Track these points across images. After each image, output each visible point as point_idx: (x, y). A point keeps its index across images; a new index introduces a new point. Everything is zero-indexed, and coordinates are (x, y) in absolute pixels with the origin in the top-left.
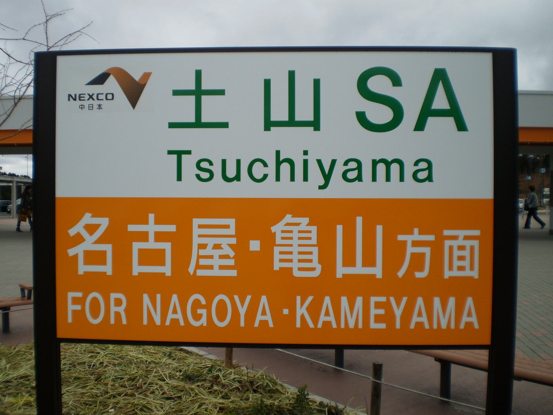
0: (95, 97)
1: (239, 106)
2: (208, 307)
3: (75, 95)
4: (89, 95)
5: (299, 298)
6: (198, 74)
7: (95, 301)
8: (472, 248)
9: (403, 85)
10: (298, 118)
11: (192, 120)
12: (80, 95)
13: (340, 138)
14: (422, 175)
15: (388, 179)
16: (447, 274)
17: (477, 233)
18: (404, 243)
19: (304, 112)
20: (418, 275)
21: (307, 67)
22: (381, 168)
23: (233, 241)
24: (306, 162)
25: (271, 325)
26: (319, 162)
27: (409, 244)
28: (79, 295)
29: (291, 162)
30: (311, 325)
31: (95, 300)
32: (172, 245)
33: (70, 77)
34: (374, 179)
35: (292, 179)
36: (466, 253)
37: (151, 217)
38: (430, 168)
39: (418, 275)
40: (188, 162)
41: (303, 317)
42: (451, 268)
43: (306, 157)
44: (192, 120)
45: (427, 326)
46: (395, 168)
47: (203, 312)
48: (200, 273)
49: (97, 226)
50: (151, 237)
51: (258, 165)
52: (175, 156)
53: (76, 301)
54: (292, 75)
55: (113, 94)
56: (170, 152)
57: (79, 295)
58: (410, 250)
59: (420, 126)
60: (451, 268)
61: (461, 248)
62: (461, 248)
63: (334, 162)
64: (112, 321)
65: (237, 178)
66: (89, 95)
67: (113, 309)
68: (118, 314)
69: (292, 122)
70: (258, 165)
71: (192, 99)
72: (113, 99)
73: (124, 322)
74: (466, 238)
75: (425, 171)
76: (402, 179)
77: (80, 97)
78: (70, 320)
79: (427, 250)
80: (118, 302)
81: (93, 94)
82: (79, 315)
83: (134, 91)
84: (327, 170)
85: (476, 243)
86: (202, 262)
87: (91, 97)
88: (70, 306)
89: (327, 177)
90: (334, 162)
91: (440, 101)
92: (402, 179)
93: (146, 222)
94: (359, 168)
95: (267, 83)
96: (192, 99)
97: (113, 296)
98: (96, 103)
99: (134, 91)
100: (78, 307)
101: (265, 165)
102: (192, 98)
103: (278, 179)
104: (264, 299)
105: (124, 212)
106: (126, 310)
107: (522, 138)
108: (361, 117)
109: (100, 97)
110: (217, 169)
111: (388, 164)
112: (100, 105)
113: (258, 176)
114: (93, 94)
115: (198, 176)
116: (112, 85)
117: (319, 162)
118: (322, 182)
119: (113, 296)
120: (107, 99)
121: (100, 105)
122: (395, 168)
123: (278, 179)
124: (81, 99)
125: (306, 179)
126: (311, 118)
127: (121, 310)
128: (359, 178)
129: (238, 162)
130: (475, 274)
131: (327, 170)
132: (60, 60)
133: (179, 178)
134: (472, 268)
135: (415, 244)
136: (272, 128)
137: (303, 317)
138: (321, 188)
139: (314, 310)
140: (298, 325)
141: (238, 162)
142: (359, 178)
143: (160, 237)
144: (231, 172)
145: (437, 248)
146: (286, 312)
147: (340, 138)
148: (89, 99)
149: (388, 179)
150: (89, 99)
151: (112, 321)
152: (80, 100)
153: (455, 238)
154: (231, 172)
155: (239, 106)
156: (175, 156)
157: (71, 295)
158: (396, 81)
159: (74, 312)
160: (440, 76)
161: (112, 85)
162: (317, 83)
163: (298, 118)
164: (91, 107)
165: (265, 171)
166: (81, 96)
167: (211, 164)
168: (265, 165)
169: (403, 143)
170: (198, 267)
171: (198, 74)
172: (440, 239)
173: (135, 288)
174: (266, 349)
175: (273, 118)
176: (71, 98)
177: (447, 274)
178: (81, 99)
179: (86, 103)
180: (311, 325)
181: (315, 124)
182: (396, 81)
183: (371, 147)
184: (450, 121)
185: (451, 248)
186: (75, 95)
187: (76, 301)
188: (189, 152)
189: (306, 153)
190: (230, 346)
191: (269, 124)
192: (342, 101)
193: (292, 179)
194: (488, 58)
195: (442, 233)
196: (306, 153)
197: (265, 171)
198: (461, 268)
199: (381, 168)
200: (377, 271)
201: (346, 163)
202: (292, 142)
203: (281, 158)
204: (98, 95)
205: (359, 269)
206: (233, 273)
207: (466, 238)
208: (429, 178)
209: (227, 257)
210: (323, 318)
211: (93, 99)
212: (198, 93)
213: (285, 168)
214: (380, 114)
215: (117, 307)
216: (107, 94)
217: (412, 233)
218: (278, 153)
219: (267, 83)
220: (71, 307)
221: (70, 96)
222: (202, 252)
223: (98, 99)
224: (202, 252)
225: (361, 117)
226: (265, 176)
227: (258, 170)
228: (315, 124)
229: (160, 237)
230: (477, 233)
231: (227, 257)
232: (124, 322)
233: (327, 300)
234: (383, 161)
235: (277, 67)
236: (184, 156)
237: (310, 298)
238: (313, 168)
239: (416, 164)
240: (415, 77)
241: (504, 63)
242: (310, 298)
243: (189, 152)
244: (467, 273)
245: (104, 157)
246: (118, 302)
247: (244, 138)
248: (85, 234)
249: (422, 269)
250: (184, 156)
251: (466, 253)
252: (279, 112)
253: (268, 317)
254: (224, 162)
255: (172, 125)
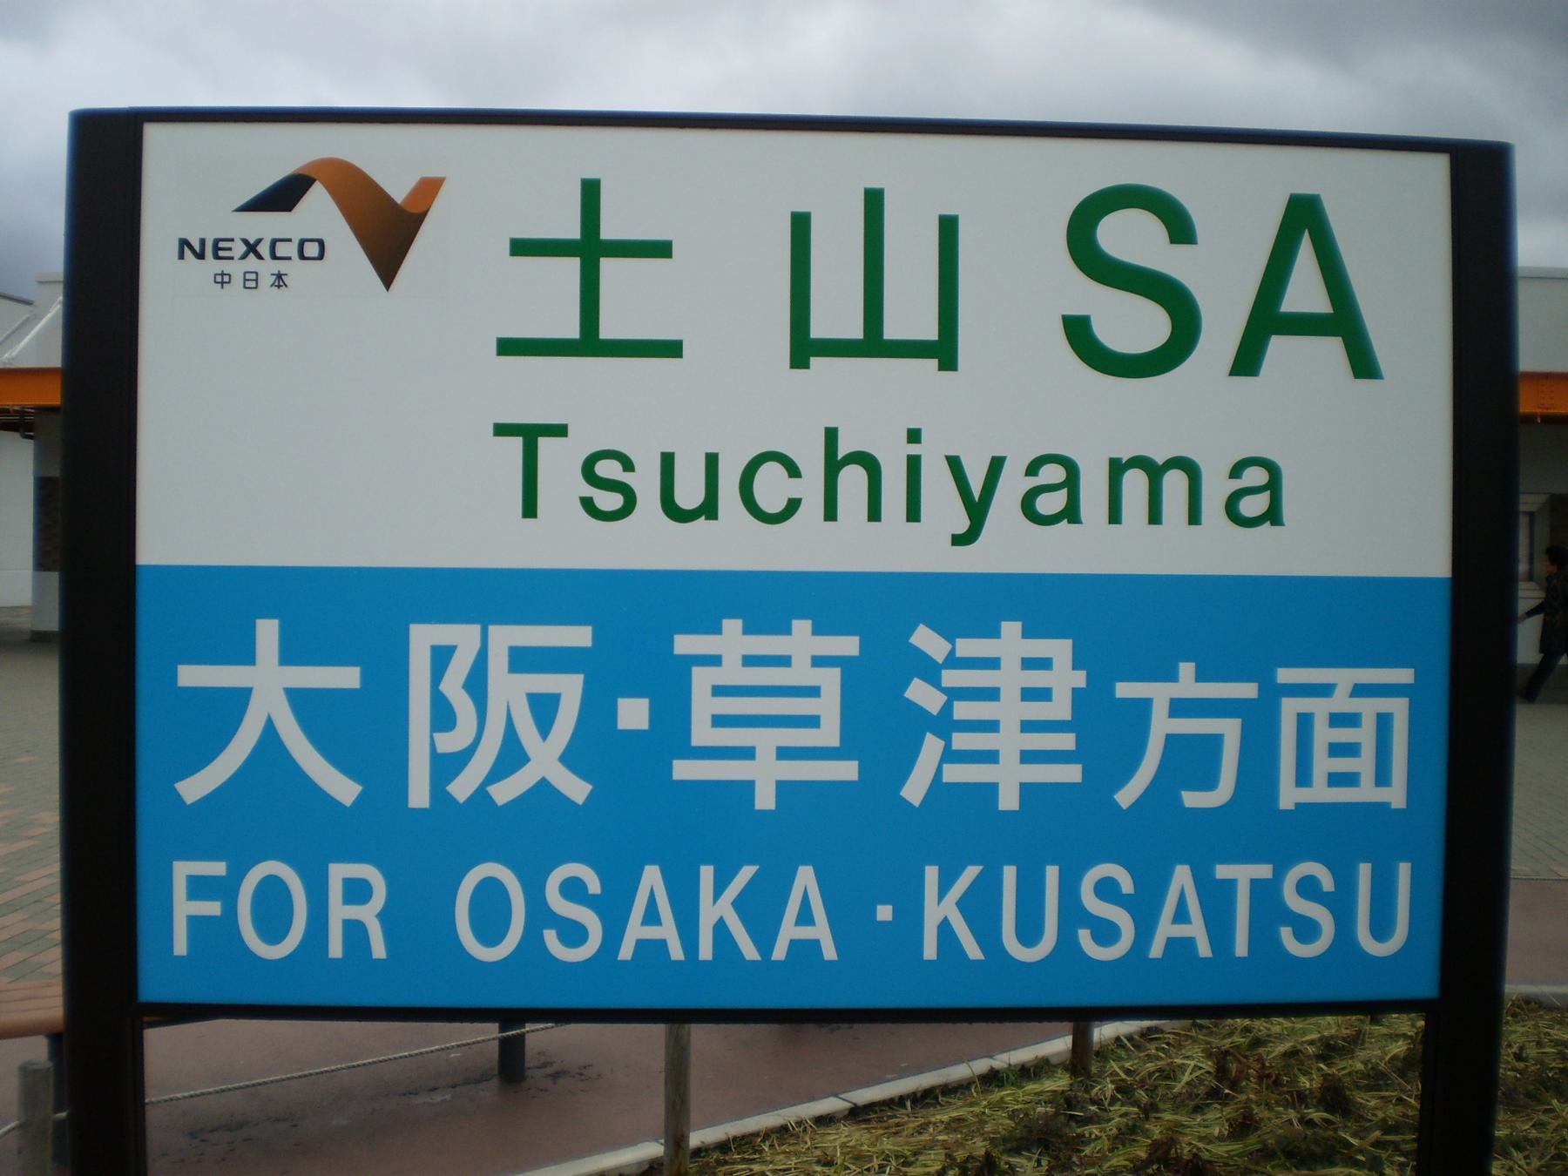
0: (264, 249)
1: (713, 288)
3: (203, 242)
4: (245, 242)
5: (931, 874)
6: (591, 192)
7: (272, 891)
8: (1384, 721)
9: (1199, 239)
10: (891, 332)
11: (572, 331)
12: (217, 241)
13: (1017, 393)
14: (1253, 506)
15: (1155, 517)
16: (1289, 796)
17: (1404, 676)
18: (1143, 707)
19: (909, 316)
20: (1192, 799)
21: (920, 179)
22: (1135, 484)
24: (914, 464)
25: (829, 952)
26: (954, 464)
27: (1159, 712)
28: (218, 868)
29: (870, 464)
30: (750, 952)
31: (491, 887)
32: (651, 704)
33: (181, 191)
34: (1115, 516)
35: (874, 514)
36: (1361, 735)
37: (268, 632)
38: (1274, 485)
39: (1192, 799)
40: (559, 463)
41: (945, 928)
42: (1303, 777)
43: (914, 449)
44: (572, 331)
45: (676, 952)
46: (1175, 483)
51: (771, 470)
52: (517, 442)
53: (200, 888)
54: (874, 202)
55: (321, 243)
56: (502, 430)
57: (218, 868)
58: (1161, 726)
59: (1247, 362)
60: (1303, 777)
63: (996, 465)
64: (336, 949)
65: (709, 509)
66: (245, 242)
67: (339, 912)
68: (354, 931)
69: (873, 344)
70: (771, 470)
71: (571, 266)
72: (321, 257)
73: (379, 950)
74: (1359, 691)
75: (1262, 495)
76: (1194, 517)
77: (216, 249)
78: (181, 946)
79: (1229, 730)
80: (357, 892)
81: (259, 241)
82: (215, 935)
83: (388, 232)
84: (976, 489)
85: (1398, 708)
87: (252, 248)
88: (182, 902)
89: (977, 510)
90: (996, 465)
91: (1305, 292)
92: (1194, 517)
93: (246, 656)
94: (1072, 483)
95: (801, 225)
96: (571, 266)
97: (339, 872)
98: (267, 268)
99: (388, 232)
100: (213, 908)
101: (793, 471)
102: (573, 265)
103: (831, 514)
104: (805, 877)
105: (356, 613)
106: (382, 916)
107: (1528, 403)
108: (1078, 332)
109: (281, 250)
110: (646, 483)
111: (1154, 472)
112: (279, 276)
113: (772, 505)
114: (259, 241)
115: (588, 504)
116: (319, 212)
117: (954, 464)
118: (962, 524)
119: (339, 872)
120: (302, 257)
121: (279, 276)
122: (1175, 483)
123: (831, 514)
124: (221, 253)
125: (913, 514)
126: (930, 332)
127: (368, 914)
128: (1071, 513)
129: (712, 461)
130: (1395, 795)
131: (976, 489)
132: (153, 134)
133: (530, 510)
134: (1382, 778)
135: (1179, 708)
136: (812, 360)
137: (945, 928)
138: (958, 540)
139: (761, 909)
140: (930, 951)
141: (712, 461)
142: (1071, 513)
144: (689, 494)
146: (884, 913)
147: (1017, 393)
148: (244, 257)
149: (1155, 517)
150: (244, 257)
151: (336, 949)
152: (217, 257)
153: (1325, 690)
154: (689, 494)
155: (713, 288)
156: (517, 442)
157: (183, 870)
158: (1180, 229)
159: (194, 922)
160: (1303, 217)
161: (319, 212)
162: (948, 228)
163: (891, 332)
164: (251, 282)
165: (793, 488)
166: (221, 245)
167: (628, 465)
168: (793, 471)
169: (1197, 413)
171: (591, 192)
172: (1272, 694)
173: (425, 849)
174: (963, 1027)
175: (818, 331)
176: (197, 248)
177: (1289, 796)
178: (221, 253)
179: (236, 268)
180: (750, 952)
181: (944, 351)
182: (1180, 229)
183: (1111, 421)
184: (1331, 349)
185: (1305, 722)
186: (203, 242)
187: (200, 888)
188: (560, 431)
189: (914, 436)
190: (676, 1017)
191: (804, 349)
192: (1022, 287)
193: (874, 514)
194: (1439, 166)
195: (1273, 676)
196: (914, 436)
197: (793, 488)
198: (1336, 780)
199: (1135, 484)
201: (1032, 469)
202: (873, 403)
203: (842, 452)
204: (274, 243)
207: (1359, 691)
208: (1273, 515)
210: (789, 931)
211: (260, 257)
212: (591, 249)
213: (853, 480)
214: (1135, 325)
215: (355, 907)
216: (302, 243)
217: (1172, 676)
218: (831, 435)
219: (801, 225)
220: (184, 908)
221: (184, 243)
223: (274, 257)
225: (1078, 332)
226: (793, 506)
227: (772, 488)
228: (944, 351)
230: (1404, 676)
232: (379, 950)
233: (652, 877)
234: (1140, 462)
235: (830, 178)
236: (544, 443)
237: (747, 873)
238: (936, 480)
239: (1236, 472)
240: (1235, 212)
241: (1480, 183)
242: (747, 873)
243: (560, 431)
244: (1366, 792)
245: (275, 438)
246: (357, 892)
247: (728, 391)
249: (1208, 781)
250: (544, 443)
251: (1365, 735)
252: (837, 314)
253: (821, 931)
254: (668, 461)
255: (508, 347)
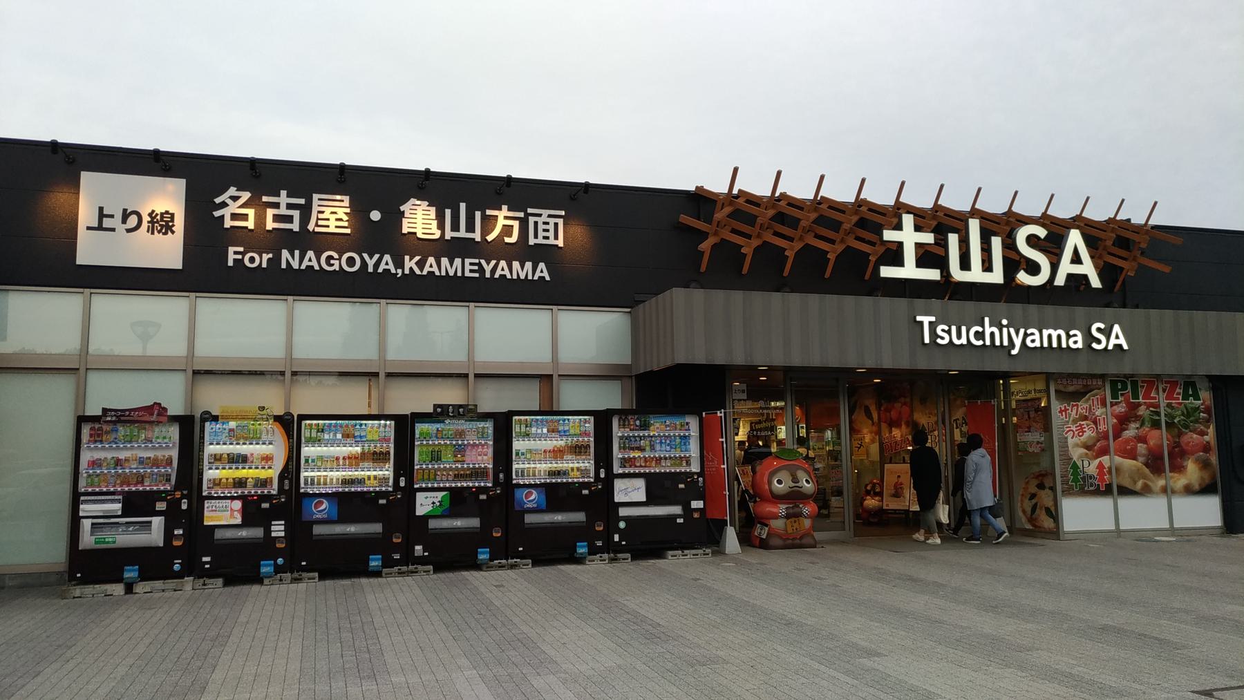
2: (340, 259)
16: (532, 241)
23: (348, 210)
39: (507, 240)
47: (336, 263)
48: (317, 229)
49: (238, 198)
50: (910, 255)
60: (536, 237)
61: (545, 223)
62: (545, 223)
74: (550, 216)
86: (320, 223)
132: (977, 206)
134: (556, 238)
143: (290, 206)
145: (524, 223)
170: (317, 225)
177: (532, 241)
185: (536, 223)
200: (997, 277)
205: (462, 233)
206: (348, 231)
209: (341, 220)
222: (321, 216)
224: (321, 216)
229: (290, 206)
231: (341, 220)
248: (229, 201)
249: (510, 236)
